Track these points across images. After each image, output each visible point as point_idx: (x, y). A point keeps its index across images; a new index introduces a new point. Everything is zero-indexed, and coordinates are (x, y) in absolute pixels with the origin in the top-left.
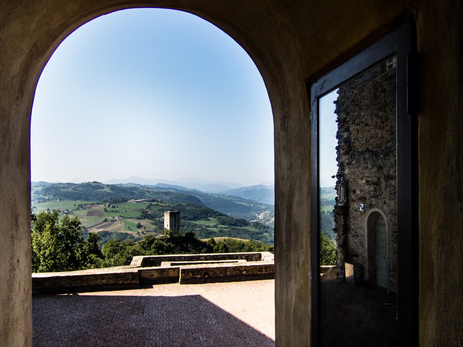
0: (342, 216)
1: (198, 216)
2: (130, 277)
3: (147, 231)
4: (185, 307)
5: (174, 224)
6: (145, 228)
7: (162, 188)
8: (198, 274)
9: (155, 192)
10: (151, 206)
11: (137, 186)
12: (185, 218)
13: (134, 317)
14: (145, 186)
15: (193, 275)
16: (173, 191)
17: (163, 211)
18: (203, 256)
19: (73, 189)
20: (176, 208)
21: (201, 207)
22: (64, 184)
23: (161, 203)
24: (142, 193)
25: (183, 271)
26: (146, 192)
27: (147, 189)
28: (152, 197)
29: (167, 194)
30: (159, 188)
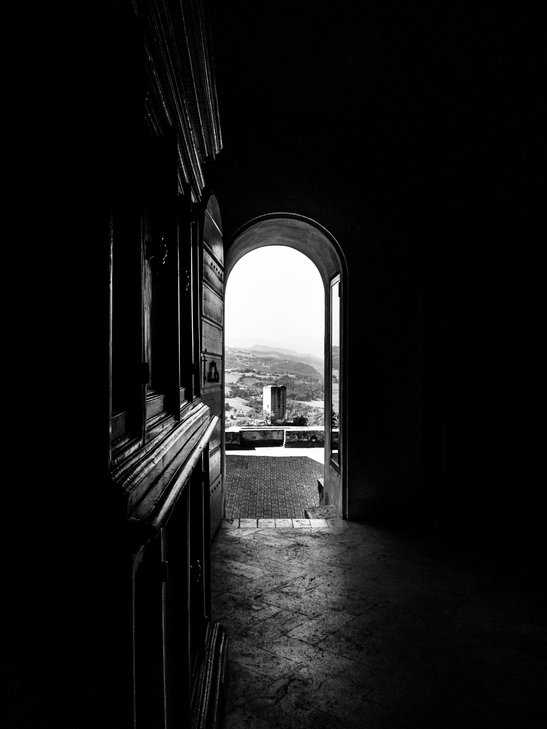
1: (313, 395)
2: (231, 438)
3: (238, 416)
4: (289, 465)
5: (277, 404)
6: (236, 410)
7: (259, 353)
8: (304, 438)
9: (250, 358)
10: (244, 379)
12: (293, 397)
14: (235, 349)
15: (299, 438)
16: (276, 356)
17: (262, 385)
20: (281, 381)
21: (318, 381)
23: (258, 373)
24: (232, 359)
25: (289, 433)
26: (238, 359)
27: (239, 354)
28: (245, 365)
29: (267, 360)
30: (255, 352)
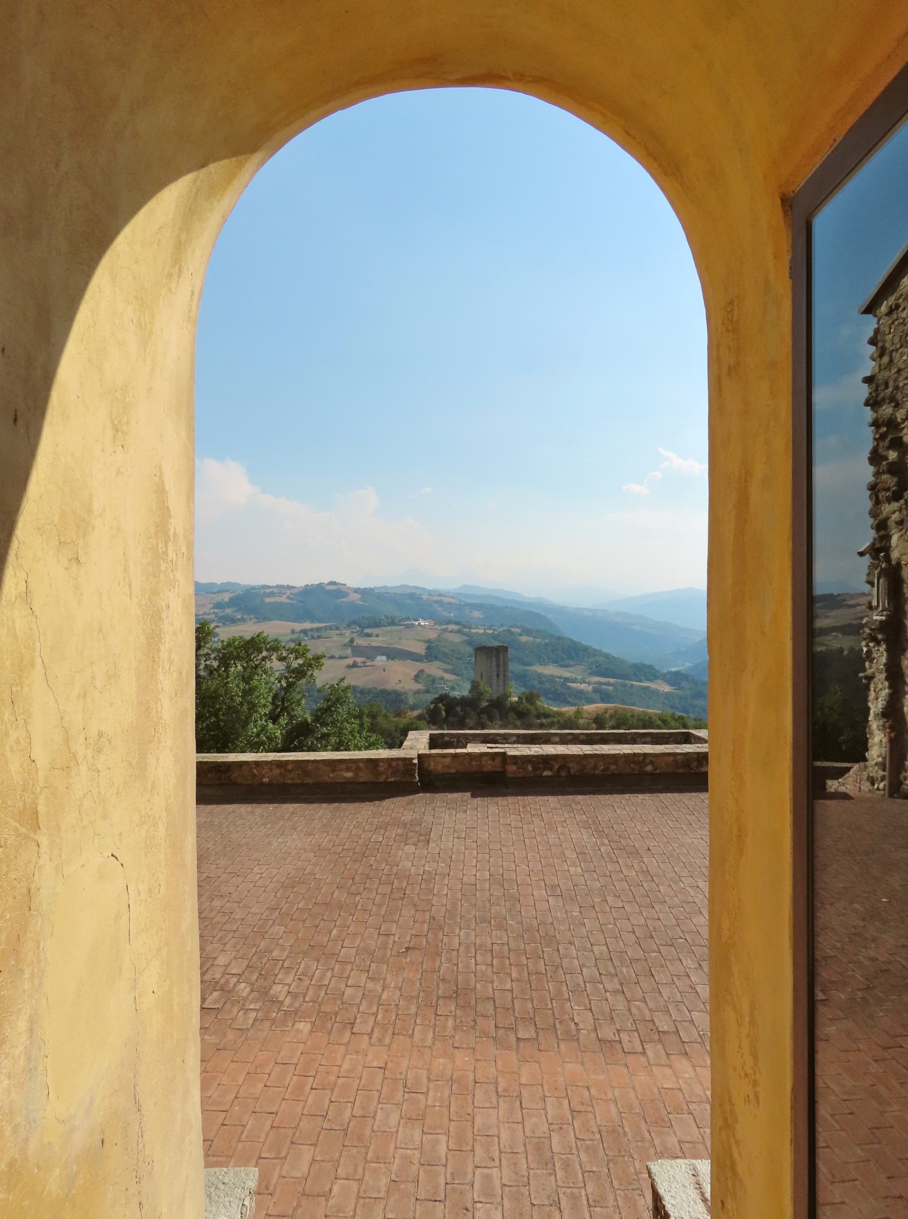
0: (883, 647)
11: (418, 592)
13: (409, 849)
18: (556, 734)
19: (288, 597)
22: (272, 587)
26: (436, 605)
